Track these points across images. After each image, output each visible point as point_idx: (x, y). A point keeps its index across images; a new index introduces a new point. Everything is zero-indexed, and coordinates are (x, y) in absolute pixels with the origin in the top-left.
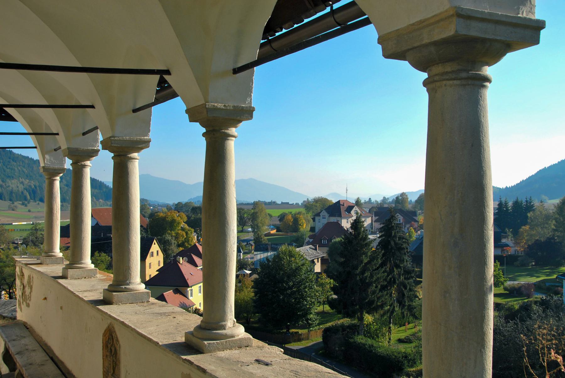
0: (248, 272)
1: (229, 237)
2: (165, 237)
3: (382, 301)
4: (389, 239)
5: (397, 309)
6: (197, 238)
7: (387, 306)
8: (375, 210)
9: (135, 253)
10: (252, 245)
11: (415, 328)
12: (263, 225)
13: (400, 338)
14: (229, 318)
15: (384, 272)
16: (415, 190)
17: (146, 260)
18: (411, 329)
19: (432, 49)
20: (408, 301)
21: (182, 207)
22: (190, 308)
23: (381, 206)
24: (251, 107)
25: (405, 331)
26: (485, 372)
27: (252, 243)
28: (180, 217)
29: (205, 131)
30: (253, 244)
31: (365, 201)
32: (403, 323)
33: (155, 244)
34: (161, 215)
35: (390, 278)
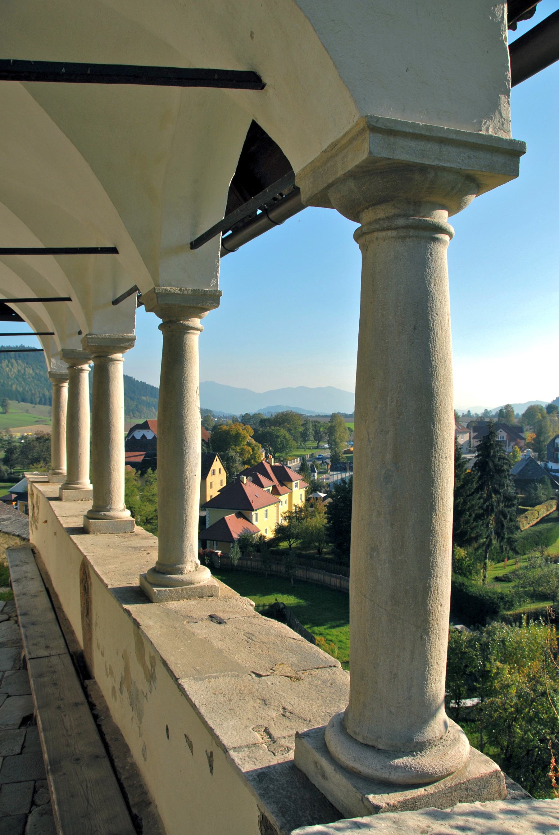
0: (323, 495)
1: (187, 457)
2: (228, 453)
3: (477, 532)
4: (487, 459)
5: (494, 542)
6: (265, 454)
7: (483, 539)
8: (474, 425)
9: (117, 473)
10: (328, 464)
11: (516, 565)
12: (342, 441)
13: (498, 576)
14: (189, 560)
15: (479, 498)
16: (523, 402)
17: (207, 479)
18: (511, 565)
19: (351, 184)
20: (508, 533)
21: (249, 419)
22: (254, 534)
23: (481, 420)
24: (216, 291)
25: (504, 567)
26: (429, 668)
27: (328, 461)
28: (246, 431)
29: (162, 322)
30: (330, 463)
31: (463, 413)
32: (501, 558)
33: (217, 461)
34: (224, 428)
35: (487, 505)
